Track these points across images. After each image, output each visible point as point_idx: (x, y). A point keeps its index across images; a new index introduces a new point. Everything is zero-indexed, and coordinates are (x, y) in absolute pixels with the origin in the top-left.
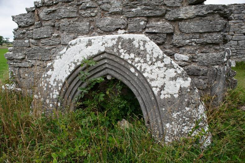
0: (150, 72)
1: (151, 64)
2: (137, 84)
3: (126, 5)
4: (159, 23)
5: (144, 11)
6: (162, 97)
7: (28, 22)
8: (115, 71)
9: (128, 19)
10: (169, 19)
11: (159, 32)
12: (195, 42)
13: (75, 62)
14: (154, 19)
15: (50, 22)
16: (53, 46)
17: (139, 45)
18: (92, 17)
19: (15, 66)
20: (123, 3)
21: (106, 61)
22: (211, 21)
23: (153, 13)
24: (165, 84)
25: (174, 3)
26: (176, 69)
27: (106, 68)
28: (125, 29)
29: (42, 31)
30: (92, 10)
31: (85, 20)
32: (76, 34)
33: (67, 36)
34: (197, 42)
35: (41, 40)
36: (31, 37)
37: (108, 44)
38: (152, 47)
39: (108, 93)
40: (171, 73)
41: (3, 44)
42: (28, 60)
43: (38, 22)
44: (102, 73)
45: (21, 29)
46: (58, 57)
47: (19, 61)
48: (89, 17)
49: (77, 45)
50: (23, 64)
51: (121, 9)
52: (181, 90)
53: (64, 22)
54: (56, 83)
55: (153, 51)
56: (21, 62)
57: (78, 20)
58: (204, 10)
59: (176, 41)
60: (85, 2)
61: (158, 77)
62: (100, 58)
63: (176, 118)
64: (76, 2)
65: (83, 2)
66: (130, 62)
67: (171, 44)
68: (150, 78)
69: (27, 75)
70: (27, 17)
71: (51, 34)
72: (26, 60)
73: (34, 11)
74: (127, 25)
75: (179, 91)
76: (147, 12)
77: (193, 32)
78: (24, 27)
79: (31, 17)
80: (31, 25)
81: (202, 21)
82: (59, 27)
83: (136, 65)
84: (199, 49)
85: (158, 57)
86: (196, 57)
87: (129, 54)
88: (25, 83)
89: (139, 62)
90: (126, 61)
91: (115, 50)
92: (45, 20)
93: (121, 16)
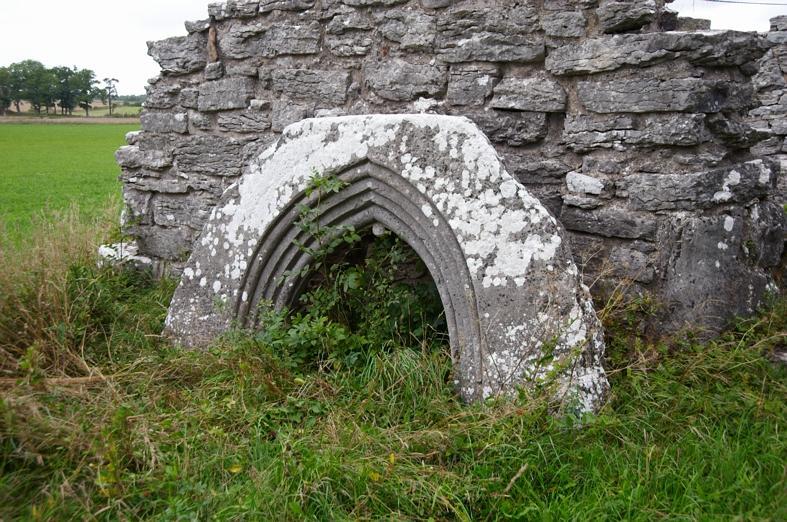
0: (465, 217)
1: (471, 196)
2: (437, 250)
3: (444, 27)
4: (525, 82)
5: (490, 47)
6: (486, 283)
7: (188, 62)
8: (392, 214)
9: (448, 68)
10: (553, 72)
11: (524, 108)
12: (623, 140)
13: (294, 183)
14: (516, 70)
15: (245, 66)
16: (251, 136)
17: (449, 145)
18: (356, 56)
19: (142, 188)
20: (437, 20)
21: (369, 184)
22: (663, 81)
23: (511, 53)
24: (496, 249)
25: (565, 27)
26: (528, 211)
27: (370, 204)
28: (439, 96)
29: (223, 89)
30: (358, 38)
31: (339, 64)
32: (314, 103)
33: (288, 108)
34: (628, 141)
35: (219, 114)
36: (192, 104)
37: (375, 138)
38: (478, 151)
39: (361, 274)
40: (515, 221)
41: (93, 105)
42: (178, 173)
43: (213, 64)
44: (359, 217)
45: (167, 79)
46: (253, 167)
47: (153, 174)
48: (348, 57)
49: (302, 138)
50: (165, 184)
51: (431, 38)
52: (532, 267)
53: (284, 67)
54: (241, 236)
55: (478, 164)
56: (158, 178)
57: (320, 62)
58: (642, 49)
59: (571, 136)
60: (340, 14)
61: (483, 229)
62: (356, 175)
63: (513, 339)
64: (319, 13)
65: (336, 14)
66: (422, 188)
67: (560, 144)
68: (464, 233)
69: (171, 217)
70: (187, 46)
71: (248, 102)
72: (175, 172)
73: (205, 32)
74: (446, 84)
75: (527, 269)
76: (496, 50)
77: (615, 111)
78: (177, 75)
79: (196, 48)
80: (196, 71)
81: (637, 79)
82: (269, 80)
83: (435, 198)
84: (632, 159)
85: (488, 179)
86: (622, 184)
87: (424, 169)
88: (164, 241)
89: (444, 189)
90: (413, 186)
91: (391, 156)
92: (234, 59)
93: (431, 58)
